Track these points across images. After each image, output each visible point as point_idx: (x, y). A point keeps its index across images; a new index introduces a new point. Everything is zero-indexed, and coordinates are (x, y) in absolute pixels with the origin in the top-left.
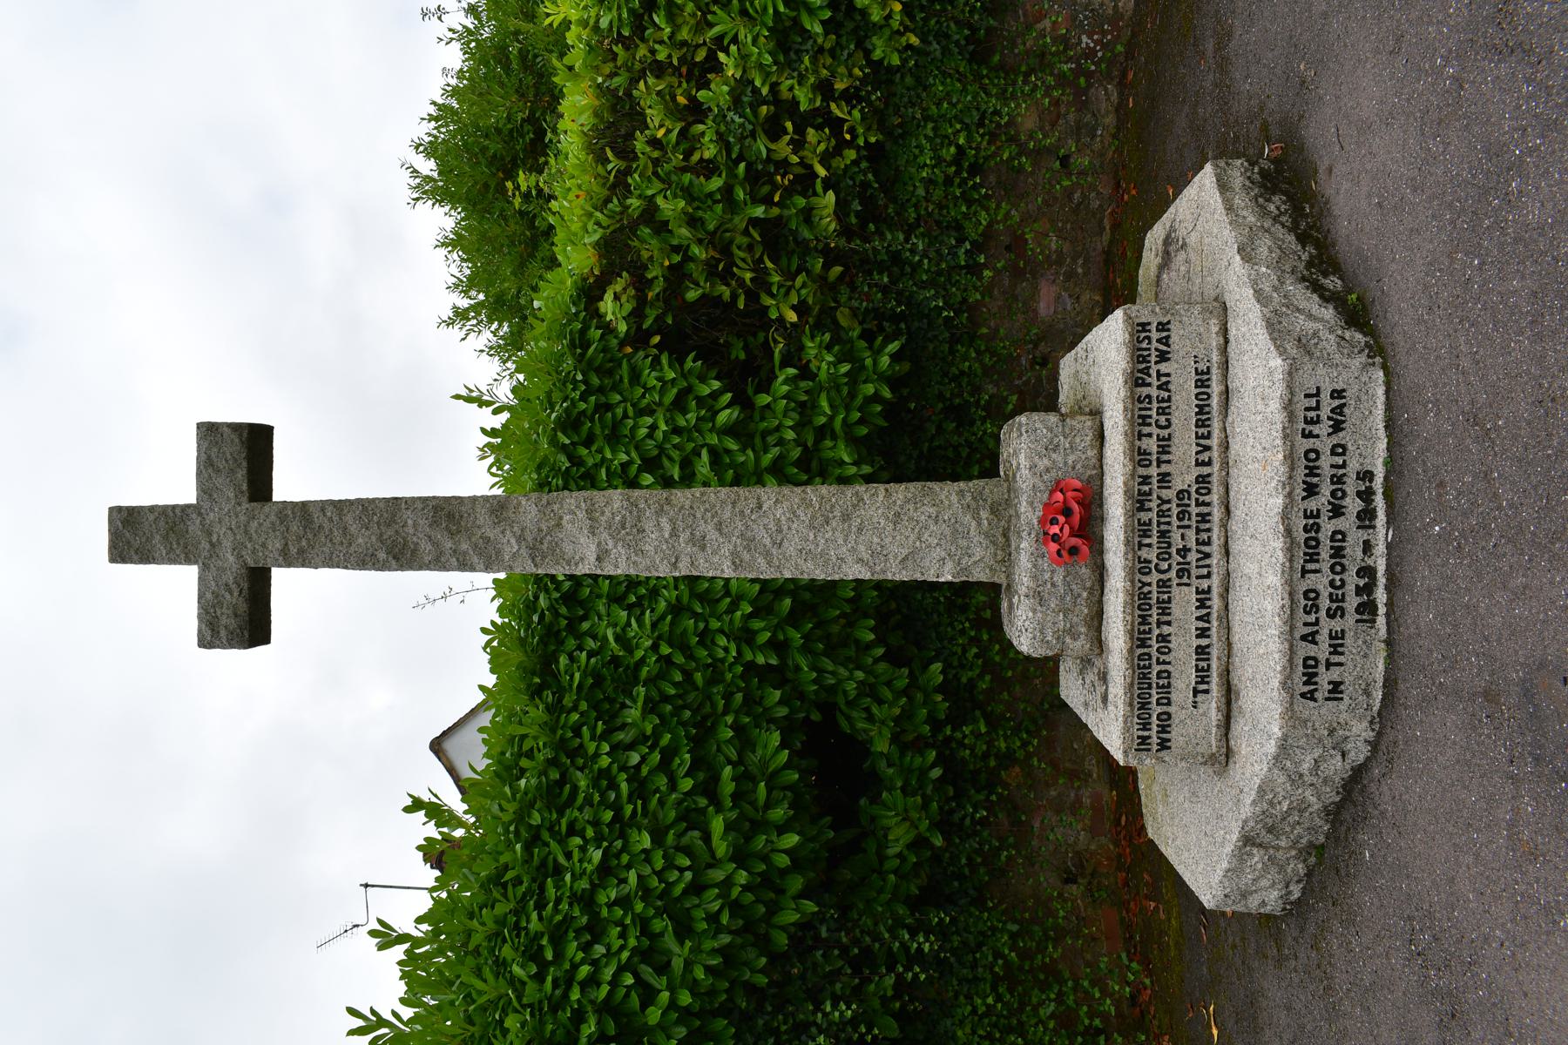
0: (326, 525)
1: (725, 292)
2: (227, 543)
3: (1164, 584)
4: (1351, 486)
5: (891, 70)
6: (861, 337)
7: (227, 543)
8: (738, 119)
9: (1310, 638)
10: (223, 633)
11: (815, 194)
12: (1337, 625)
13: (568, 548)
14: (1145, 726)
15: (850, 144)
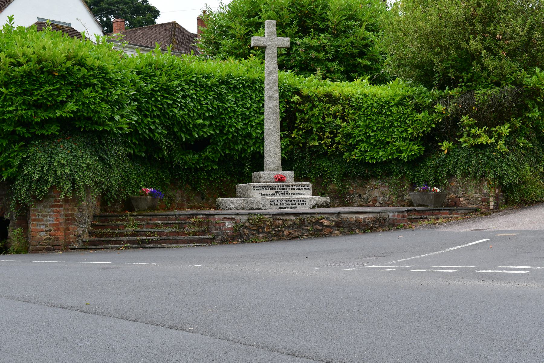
0: (273, 61)
1: (297, 122)
2: (270, 43)
3: (276, 189)
4: (295, 206)
5: (343, 156)
6: (288, 151)
7: (270, 43)
8: (333, 126)
9: (277, 201)
10: (256, 42)
11: (318, 141)
12: (279, 204)
13: (271, 102)
14: (257, 187)
15: (328, 148)
